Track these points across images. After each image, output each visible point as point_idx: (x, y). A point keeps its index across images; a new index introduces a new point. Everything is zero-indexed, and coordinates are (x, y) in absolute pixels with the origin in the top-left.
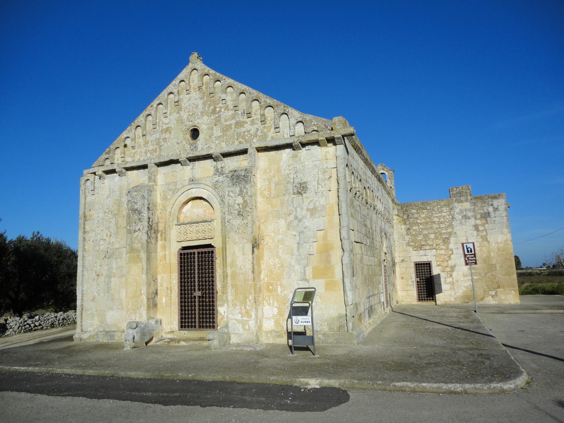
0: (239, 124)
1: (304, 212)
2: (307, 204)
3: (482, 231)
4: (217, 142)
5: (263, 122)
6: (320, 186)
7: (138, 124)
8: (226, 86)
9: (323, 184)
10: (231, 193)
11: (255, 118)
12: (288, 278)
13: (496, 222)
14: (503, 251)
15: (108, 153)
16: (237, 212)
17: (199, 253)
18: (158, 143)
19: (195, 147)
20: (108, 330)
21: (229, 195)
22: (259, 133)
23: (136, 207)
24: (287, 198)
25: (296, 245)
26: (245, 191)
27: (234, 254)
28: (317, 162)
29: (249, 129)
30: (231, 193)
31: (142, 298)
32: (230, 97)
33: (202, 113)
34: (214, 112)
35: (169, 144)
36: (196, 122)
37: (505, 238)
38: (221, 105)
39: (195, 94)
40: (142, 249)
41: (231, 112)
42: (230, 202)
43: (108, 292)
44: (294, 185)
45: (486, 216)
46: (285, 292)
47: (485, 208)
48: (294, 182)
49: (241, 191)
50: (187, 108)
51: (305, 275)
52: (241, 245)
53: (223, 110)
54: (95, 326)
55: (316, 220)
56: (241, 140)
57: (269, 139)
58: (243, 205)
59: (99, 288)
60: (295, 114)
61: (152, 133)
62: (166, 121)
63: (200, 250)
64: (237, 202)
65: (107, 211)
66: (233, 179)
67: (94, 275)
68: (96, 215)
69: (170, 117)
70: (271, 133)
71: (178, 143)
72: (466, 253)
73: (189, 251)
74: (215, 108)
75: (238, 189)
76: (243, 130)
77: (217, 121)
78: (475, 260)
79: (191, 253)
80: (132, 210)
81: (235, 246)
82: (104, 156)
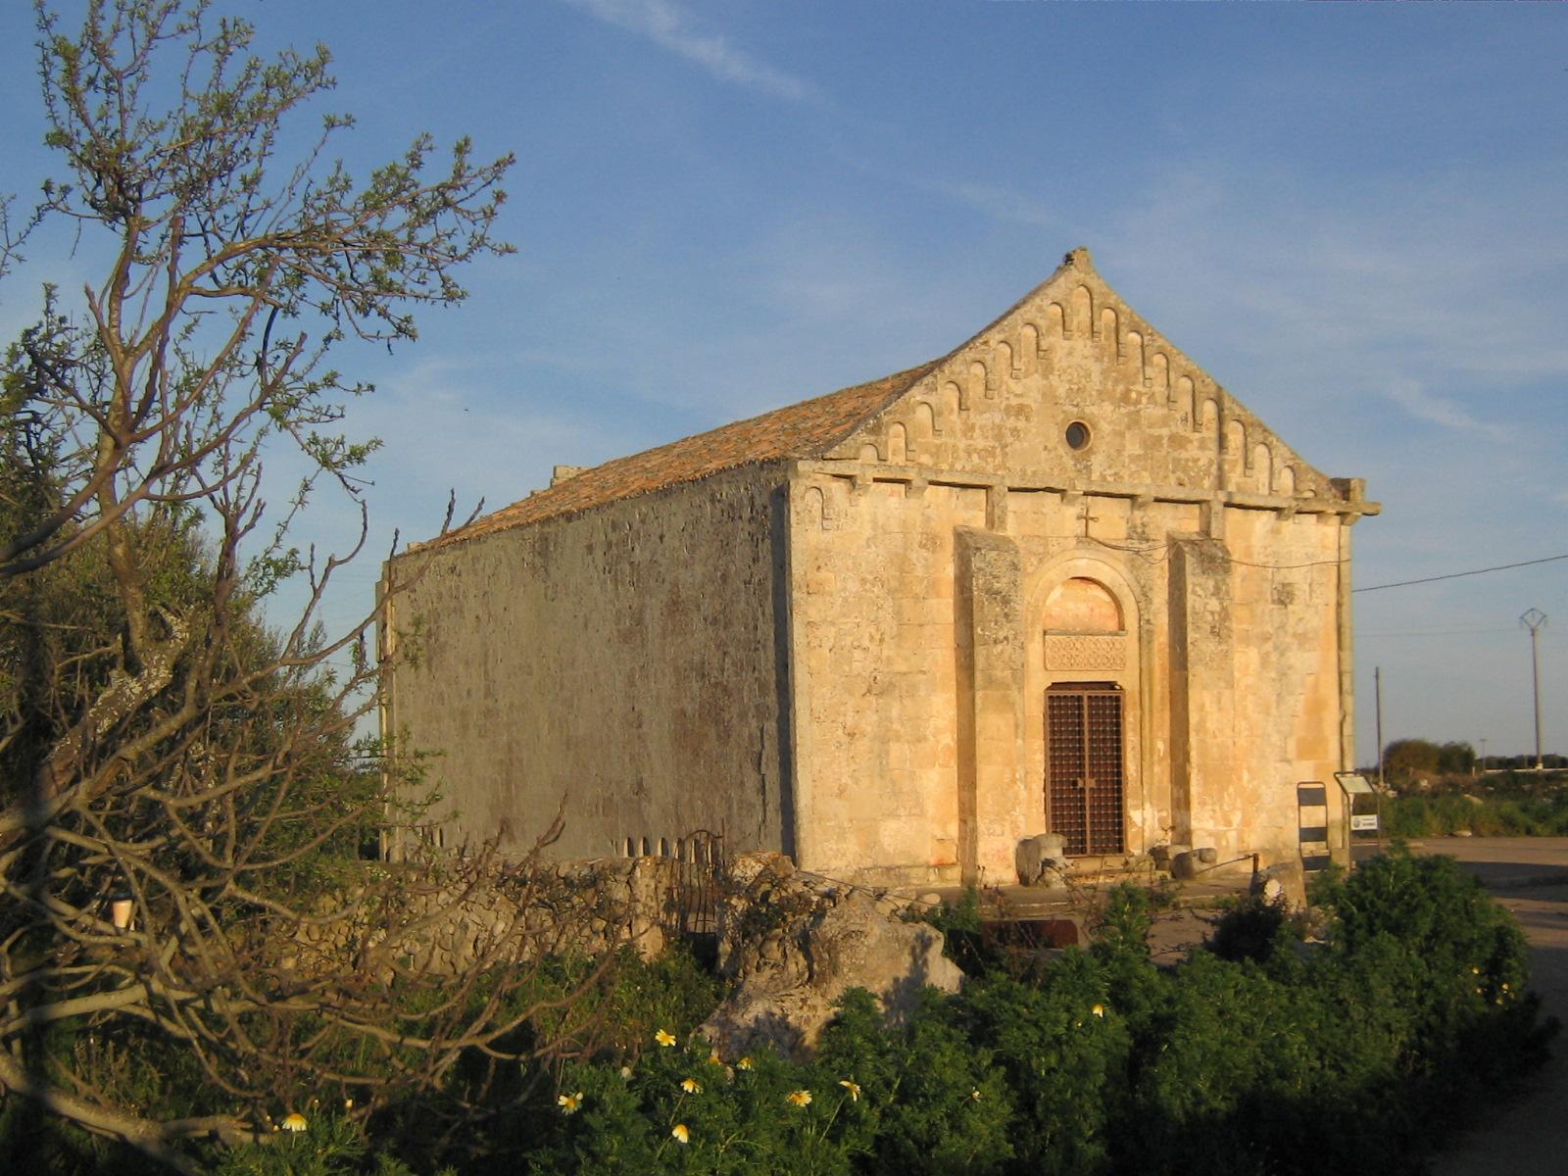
0: (1177, 441)
4: (1133, 467)
16: (1208, 628)
18: (999, 437)
21: (1194, 592)
23: (997, 586)
25: (1274, 698)
27: (1202, 707)
33: (1100, 392)
34: (1125, 398)
38: (1139, 388)
39: (1082, 346)
53: (1144, 400)
54: (850, 857)
59: (854, 767)
62: (1017, 388)
65: (871, 578)
74: (1128, 391)
75: (1211, 584)
77: (1134, 421)
81: (1205, 693)
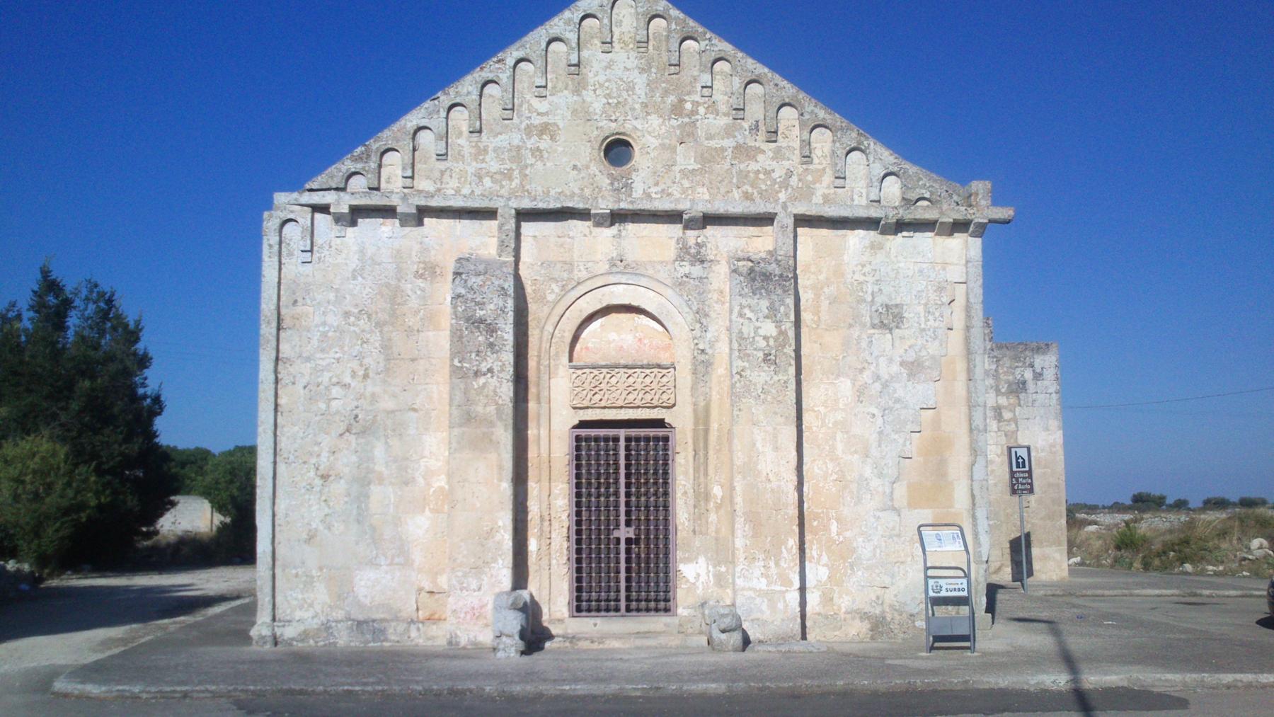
1: (895, 368)
2: (902, 351)
3: (1009, 421)
4: (686, 184)
5: (807, 158)
6: (931, 317)
7: (458, 100)
8: (714, 56)
9: (937, 314)
10: (747, 311)
11: (784, 145)
12: (856, 504)
13: (1037, 404)
14: (1045, 467)
15: (358, 159)
16: (761, 354)
17: (628, 439)
19: (626, 185)
20: (361, 617)
21: (741, 315)
22: (794, 181)
23: (480, 313)
24: (857, 333)
25: (875, 436)
26: (782, 309)
28: (925, 266)
29: (768, 168)
30: (747, 311)
31: (498, 537)
32: (725, 81)
33: (645, 105)
34: (677, 109)
35: (548, 164)
36: (628, 126)
37: (1051, 439)
38: (697, 98)
39: (625, 58)
40: (500, 418)
41: (724, 121)
42: (745, 330)
43: (358, 521)
44: (874, 308)
45: (1019, 388)
46: (848, 534)
47: (1018, 371)
48: (873, 301)
49: (772, 308)
50: (601, 85)
51: (892, 500)
52: (770, 429)
53: (702, 110)
54: (318, 608)
55: (920, 387)
56: (747, 188)
57: (818, 199)
58: (776, 339)
59: (327, 511)
60: (885, 157)
61: (498, 129)
62: (542, 106)
63: (634, 432)
64: (761, 332)
66: (754, 280)
67: (312, 474)
68: (318, 320)
69: (554, 99)
70: (824, 187)
71: (575, 167)
72: (1015, 469)
73: (602, 432)
74: (682, 101)
75: (764, 304)
76: (753, 166)
77: (687, 135)
78: (1031, 484)
79: (606, 439)
80: (467, 320)
81: (756, 430)
82: (348, 165)
